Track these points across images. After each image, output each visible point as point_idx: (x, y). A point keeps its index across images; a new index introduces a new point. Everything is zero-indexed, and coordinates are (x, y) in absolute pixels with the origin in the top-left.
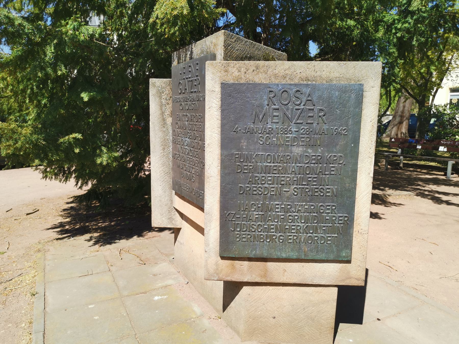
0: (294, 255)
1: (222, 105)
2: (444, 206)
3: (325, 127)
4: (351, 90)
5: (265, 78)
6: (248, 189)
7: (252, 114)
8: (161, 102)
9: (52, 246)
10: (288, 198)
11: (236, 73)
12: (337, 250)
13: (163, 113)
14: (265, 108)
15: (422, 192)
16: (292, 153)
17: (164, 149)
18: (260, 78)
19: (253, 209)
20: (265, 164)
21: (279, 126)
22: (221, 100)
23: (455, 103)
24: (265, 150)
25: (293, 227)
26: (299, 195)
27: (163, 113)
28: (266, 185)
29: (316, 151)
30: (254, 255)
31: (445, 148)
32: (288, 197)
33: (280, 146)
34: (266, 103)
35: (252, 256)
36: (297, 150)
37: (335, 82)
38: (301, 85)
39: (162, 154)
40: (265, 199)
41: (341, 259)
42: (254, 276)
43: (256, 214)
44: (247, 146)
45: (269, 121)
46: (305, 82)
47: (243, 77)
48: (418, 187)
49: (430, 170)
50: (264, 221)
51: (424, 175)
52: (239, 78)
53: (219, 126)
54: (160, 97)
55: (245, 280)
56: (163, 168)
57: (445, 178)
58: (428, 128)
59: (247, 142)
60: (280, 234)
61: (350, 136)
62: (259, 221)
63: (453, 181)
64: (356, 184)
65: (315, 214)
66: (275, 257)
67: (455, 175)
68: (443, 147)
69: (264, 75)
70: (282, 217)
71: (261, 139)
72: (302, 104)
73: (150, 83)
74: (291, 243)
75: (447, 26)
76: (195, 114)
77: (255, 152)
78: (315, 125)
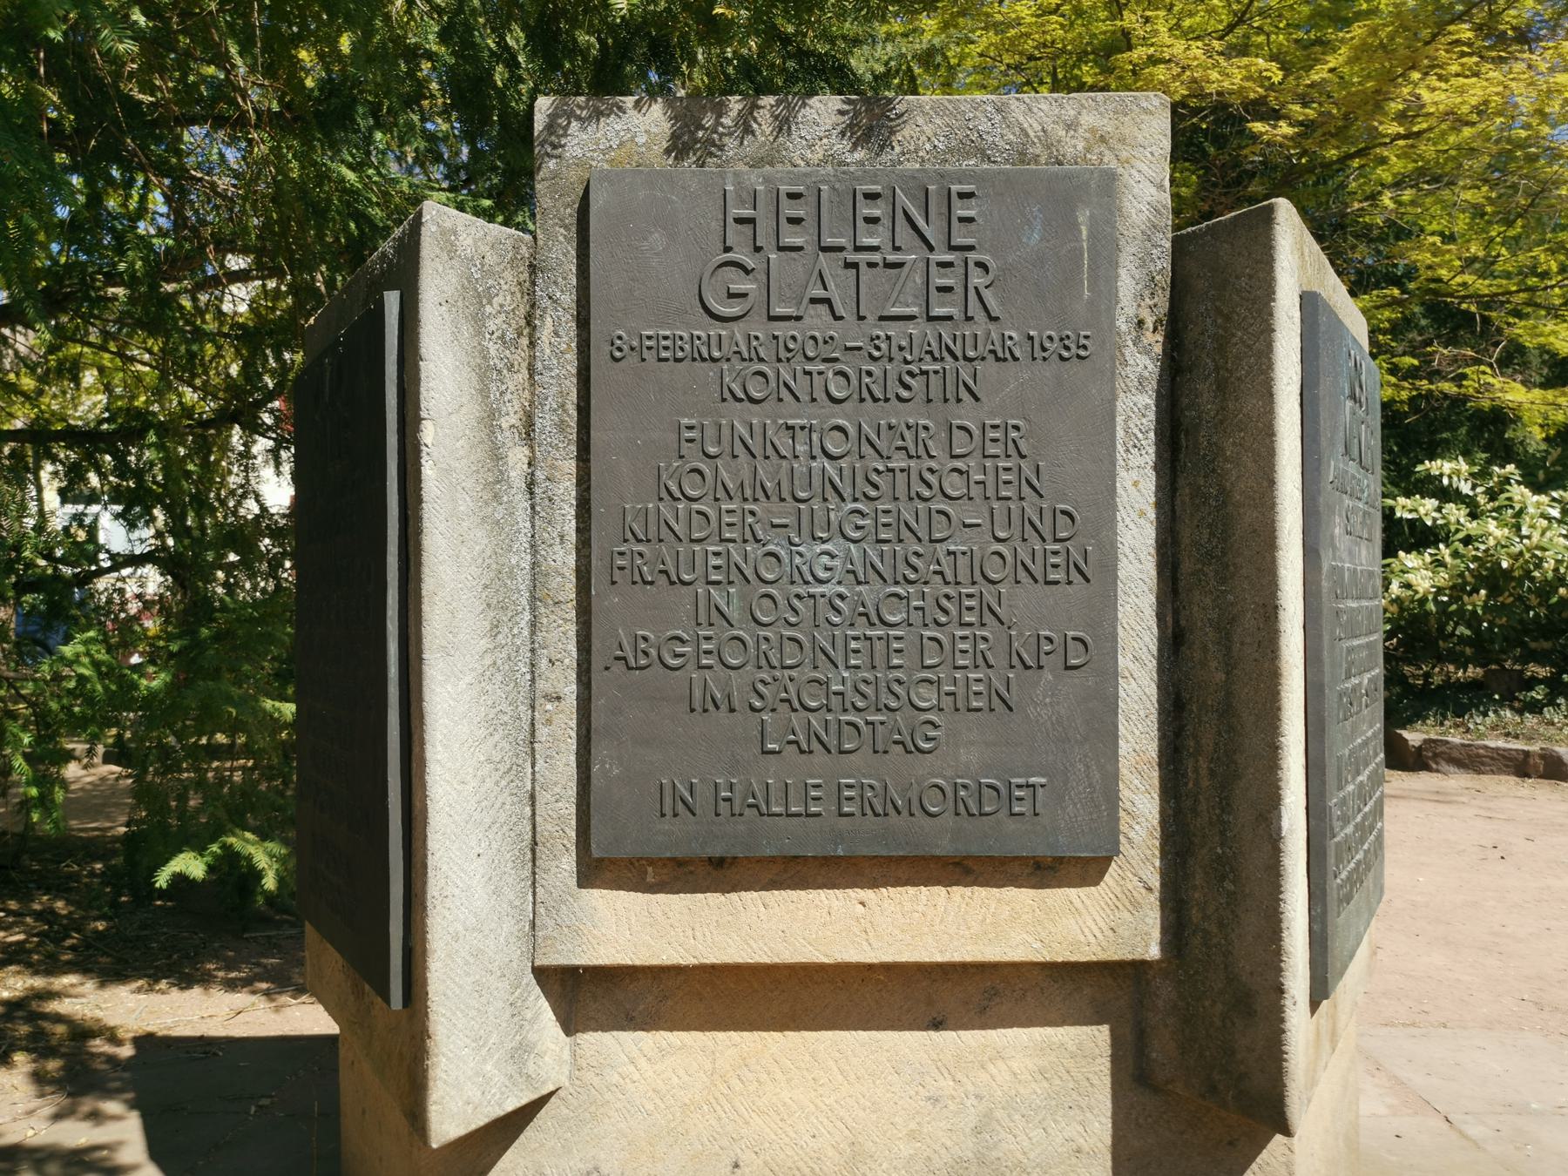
13: (491, 417)
17: (495, 628)
39: (488, 661)
54: (478, 321)
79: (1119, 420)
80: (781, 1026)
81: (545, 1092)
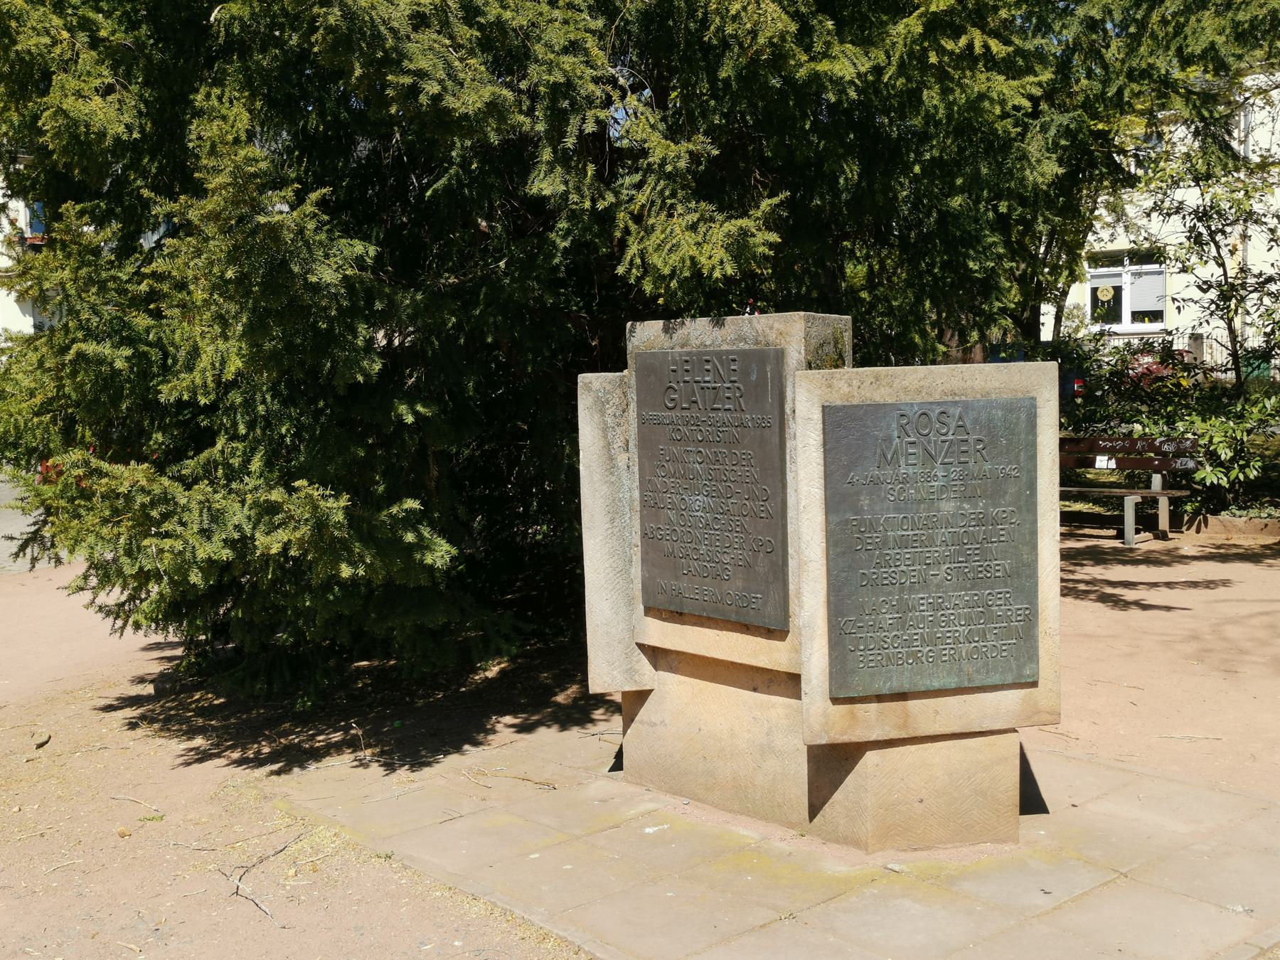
0: (952, 682)
2: (1135, 613)
3: (987, 466)
4: (1020, 408)
5: (890, 395)
6: (875, 577)
7: (875, 453)
8: (605, 423)
9: (800, 634)
10: (938, 586)
11: (846, 389)
12: (1018, 666)
13: (608, 446)
14: (894, 443)
16: (939, 511)
17: (612, 521)
18: (882, 395)
19: (884, 611)
20: (899, 533)
21: (918, 470)
23: (1108, 302)
24: (898, 510)
25: (948, 635)
26: (955, 580)
27: (609, 444)
29: (976, 506)
30: (889, 689)
31: (1110, 459)
32: (937, 585)
33: (920, 502)
34: (896, 434)
35: (885, 691)
36: (948, 507)
37: (994, 397)
38: (945, 403)
39: (610, 532)
40: (902, 591)
41: (1023, 681)
42: (887, 728)
43: (888, 618)
44: (869, 505)
45: (902, 461)
46: (950, 398)
47: (856, 393)
49: (1075, 526)
50: (903, 628)
54: (602, 412)
55: (873, 738)
56: (612, 560)
57: (1121, 545)
58: (934, 317)
59: (870, 500)
60: (928, 648)
61: (1024, 480)
62: (894, 630)
63: (1139, 552)
64: (1037, 554)
65: (981, 609)
66: (923, 689)
68: (1106, 458)
69: (888, 390)
70: (930, 619)
71: (891, 492)
72: (951, 433)
74: (945, 661)
75: (1097, 172)
76: (730, 451)
77: (882, 515)
78: (971, 464)
79: (788, 451)
80: (711, 681)
81: (1018, 751)
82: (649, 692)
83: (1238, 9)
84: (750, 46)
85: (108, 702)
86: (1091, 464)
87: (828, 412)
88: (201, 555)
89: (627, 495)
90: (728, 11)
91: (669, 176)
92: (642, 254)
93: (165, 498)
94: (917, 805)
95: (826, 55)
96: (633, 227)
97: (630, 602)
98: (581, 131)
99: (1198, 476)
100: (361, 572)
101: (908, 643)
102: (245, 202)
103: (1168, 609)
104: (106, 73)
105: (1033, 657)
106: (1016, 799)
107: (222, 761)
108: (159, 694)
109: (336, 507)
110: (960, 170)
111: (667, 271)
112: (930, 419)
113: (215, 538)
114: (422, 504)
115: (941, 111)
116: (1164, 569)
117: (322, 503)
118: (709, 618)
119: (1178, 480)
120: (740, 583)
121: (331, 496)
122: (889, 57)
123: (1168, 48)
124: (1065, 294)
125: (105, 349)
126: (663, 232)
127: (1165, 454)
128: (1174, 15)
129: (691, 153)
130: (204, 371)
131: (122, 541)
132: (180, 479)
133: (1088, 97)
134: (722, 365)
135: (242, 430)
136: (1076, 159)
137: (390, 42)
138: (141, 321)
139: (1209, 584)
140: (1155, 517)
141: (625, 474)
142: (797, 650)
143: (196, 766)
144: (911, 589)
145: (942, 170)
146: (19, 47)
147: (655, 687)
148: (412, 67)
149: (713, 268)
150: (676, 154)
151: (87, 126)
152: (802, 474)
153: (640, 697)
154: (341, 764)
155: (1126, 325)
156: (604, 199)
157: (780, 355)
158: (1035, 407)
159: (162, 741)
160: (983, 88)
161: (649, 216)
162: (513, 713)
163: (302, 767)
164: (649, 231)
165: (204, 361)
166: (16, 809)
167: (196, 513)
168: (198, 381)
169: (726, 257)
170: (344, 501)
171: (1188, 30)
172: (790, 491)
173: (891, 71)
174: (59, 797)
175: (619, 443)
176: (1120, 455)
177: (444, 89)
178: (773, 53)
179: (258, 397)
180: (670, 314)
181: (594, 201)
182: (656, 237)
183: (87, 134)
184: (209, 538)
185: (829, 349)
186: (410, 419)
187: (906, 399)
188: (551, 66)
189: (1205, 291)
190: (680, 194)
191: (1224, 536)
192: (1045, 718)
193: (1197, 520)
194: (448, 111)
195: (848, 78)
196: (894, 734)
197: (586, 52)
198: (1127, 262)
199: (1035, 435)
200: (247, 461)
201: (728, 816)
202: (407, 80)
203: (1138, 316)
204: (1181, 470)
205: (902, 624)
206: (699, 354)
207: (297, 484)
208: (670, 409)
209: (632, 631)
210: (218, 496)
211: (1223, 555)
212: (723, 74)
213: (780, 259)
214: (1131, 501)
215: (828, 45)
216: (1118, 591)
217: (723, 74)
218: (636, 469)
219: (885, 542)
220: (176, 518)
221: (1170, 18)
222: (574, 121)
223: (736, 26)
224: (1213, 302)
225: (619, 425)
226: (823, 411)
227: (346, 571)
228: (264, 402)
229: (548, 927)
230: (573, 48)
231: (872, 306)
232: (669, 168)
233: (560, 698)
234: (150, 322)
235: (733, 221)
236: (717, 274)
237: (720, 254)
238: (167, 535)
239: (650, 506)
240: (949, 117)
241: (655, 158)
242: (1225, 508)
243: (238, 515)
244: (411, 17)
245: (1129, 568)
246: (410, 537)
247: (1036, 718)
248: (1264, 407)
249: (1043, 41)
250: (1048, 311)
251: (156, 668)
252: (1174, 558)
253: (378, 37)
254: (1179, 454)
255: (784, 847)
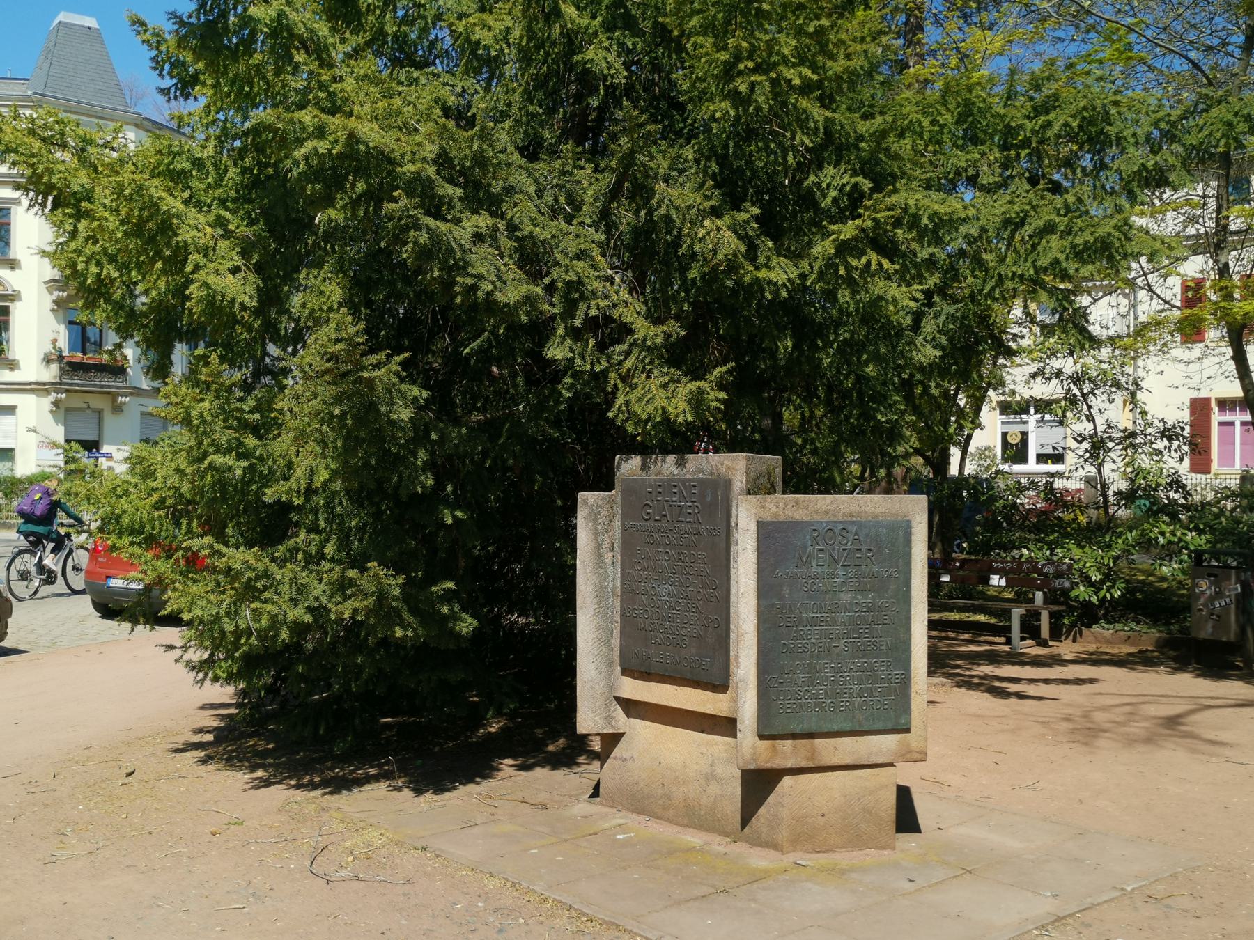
0: (847, 726)
1: (758, 549)
3: (875, 569)
8: (597, 529)
10: (838, 655)
11: (774, 510)
15: (966, 679)
17: (599, 602)
18: (800, 515)
22: (758, 541)
23: (1017, 444)
24: (810, 598)
28: (813, 641)
31: (1001, 578)
34: (809, 543)
35: (798, 731)
36: (846, 597)
38: (845, 522)
40: (812, 657)
43: (802, 677)
46: (849, 519)
48: (958, 671)
50: (812, 685)
51: (965, 645)
52: (777, 514)
53: (756, 571)
54: (595, 521)
55: (789, 766)
66: (826, 730)
67: (1029, 642)
73: (579, 500)
82: (621, 735)
83: (1075, 235)
84: (712, 259)
85: (176, 746)
86: (986, 581)
87: (761, 525)
88: (290, 617)
89: (611, 584)
90: (696, 235)
91: (649, 349)
92: (627, 404)
93: (266, 574)
94: (820, 818)
95: (767, 266)
96: (620, 385)
97: (610, 665)
98: (587, 315)
99: (1073, 594)
100: (410, 634)
101: (816, 696)
102: (351, 362)
103: (1040, 698)
104: (236, 258)
105: (907, 710)
106: (892, 812)
107: (283, 786)
108: (218, 741)
109: (395, 584)
110: (864, 349)
111: (644, 417)
112: (834, 533)
113: (300, 606)
114: (456, 585)
115: (852, 306)
116: (1046, 669)
117: (384, 581)
118: (670, 677)
119: (1057, 597)
120: (694, 650)
121: (392, 575)
122: (811, 267)
123: (1026, 260)
124: (969, 437)
125: (229, 460)
126: (643, 388)
127: (1046, 575)
128: (1031, 237)
129: (665, 333)
130: (299, 480)
131: (224, 605)
132: (273, 560)
133: (973, 291)
134: (685, 489)
135: (322, 524)
136: (964, 337)
137: (459, 255)
138: (250, 441)
139: (1078, 682)
140: (1038, 628)
141: (610, 568)
142: (735, 701)
143: (263, 789)
144: (819, 656)
145: (849, 350)
146: (180, 238)
147: (627, 731)
148: (473, 272)
149: (678, 416)
150: (654, 334)
151: (223, 295)
152: (741, 570)
153: (612, 740)
154: (379, 790)
155: (1032, 466)
156: (600, 364)
157: (728, 484)
158: (910, 527)
159: (228, 773)
160: (881, 292)
161: (633, 377)
162: (514, 757)
163: (349, 790)
164: (633, 387)
165: (299, 473)
166: (124, 816)
167: (287, 586)
168: (294, 487)
169: (688, 409)
170: (401, 580)
171: (1040, 248)
172: (733, 582)
173: (813, 277)
174: (157, 809)
175: (606, 545)
176: (1011, 575)
177: (495, 287)
178: (727, 266)
179: (337, 501)
180: (643, 450)
181: (592, 365)
182: (638, 392)
183: (222, 301)
184: (296, 605)
185: (764, 480)
186: (449, 521)
187: (817, 518)
188: (567, 269)
189: (1080, 442)
190: (656, 362)
191: (1095, 646)
192: (916, 756)
193: (1073, 632)
194: (496, 302)
195: (780, 283)
196: (804, 764)
197: (592, 258)
198: (1032, 410)
199: (910, 548)
200: (323, 546)
201: (679, 829)
202: (470, 281)
203: (1042, 458)
204: (1060, 589)
205: (811, 681)
206: (669, 481)
207: (369, 565)
208: (646, 520)
209: (611, 686)
210: (304, 575)
211: (1097, 660)
212: (691, 275)
213: (730, 410)
214: (1017, 613)
215: (768, 258)
216: (1004, 685)
217: (691, 275)
218: (619, 564)
219: (800, 621)
220: (273, 589)
221: (1027, 238)
222: (582, 306)
223: (702, 245)
224: (1087, 451)
225: (607, 531)
226: (758, 525)
227: (399, 632)
228: (341, 504)
229: (547, 894)
230: (581, 255)
231: (803, 446)
232: (649, 343)
233: (551, 748)
234: (257, 442)
235: (693, 383)
236: (680, 420)
237: (683, 405)
238: (266, 601)
239: (628, 593)
240: (857, 310)
241: (638, 336)
242: (1097, 622)
243: (318, 590)
244: (474, 236)
245: (1017, 668)
246: (445, 610)
247: (908, 756)
248: (1127, 539)
249: (935, 250)
250: (955, 453)
251: (216, 724)
252: (1058, 661)
253: (450, 251)
254: (1059, 575)
255: (721, 849)
